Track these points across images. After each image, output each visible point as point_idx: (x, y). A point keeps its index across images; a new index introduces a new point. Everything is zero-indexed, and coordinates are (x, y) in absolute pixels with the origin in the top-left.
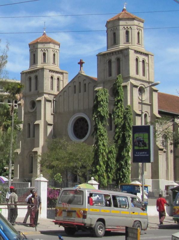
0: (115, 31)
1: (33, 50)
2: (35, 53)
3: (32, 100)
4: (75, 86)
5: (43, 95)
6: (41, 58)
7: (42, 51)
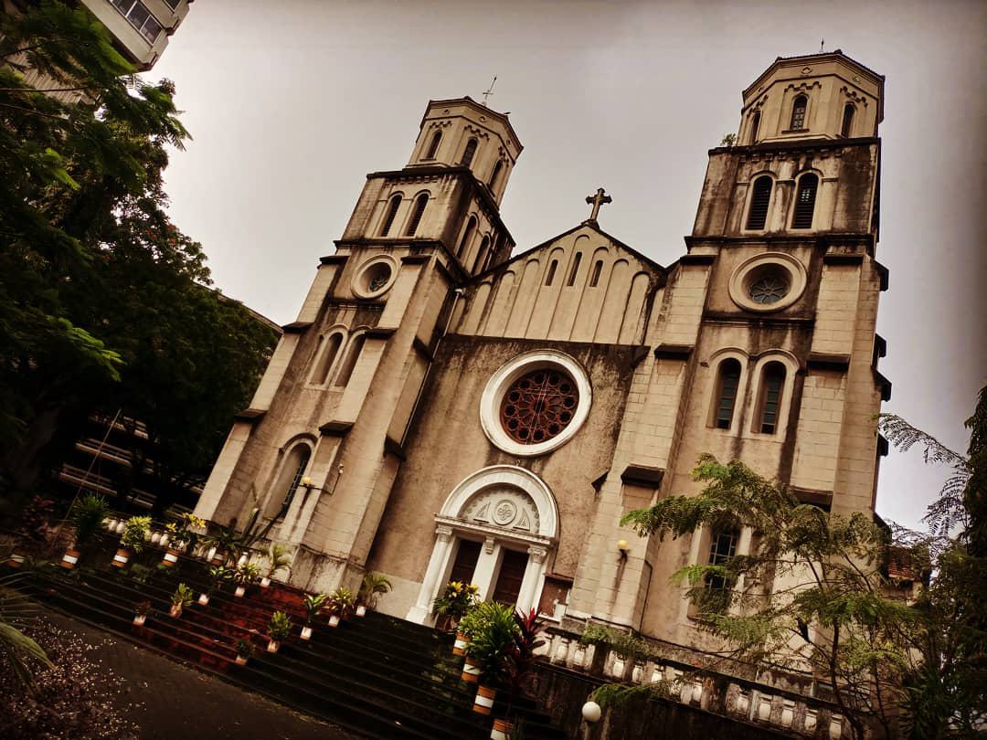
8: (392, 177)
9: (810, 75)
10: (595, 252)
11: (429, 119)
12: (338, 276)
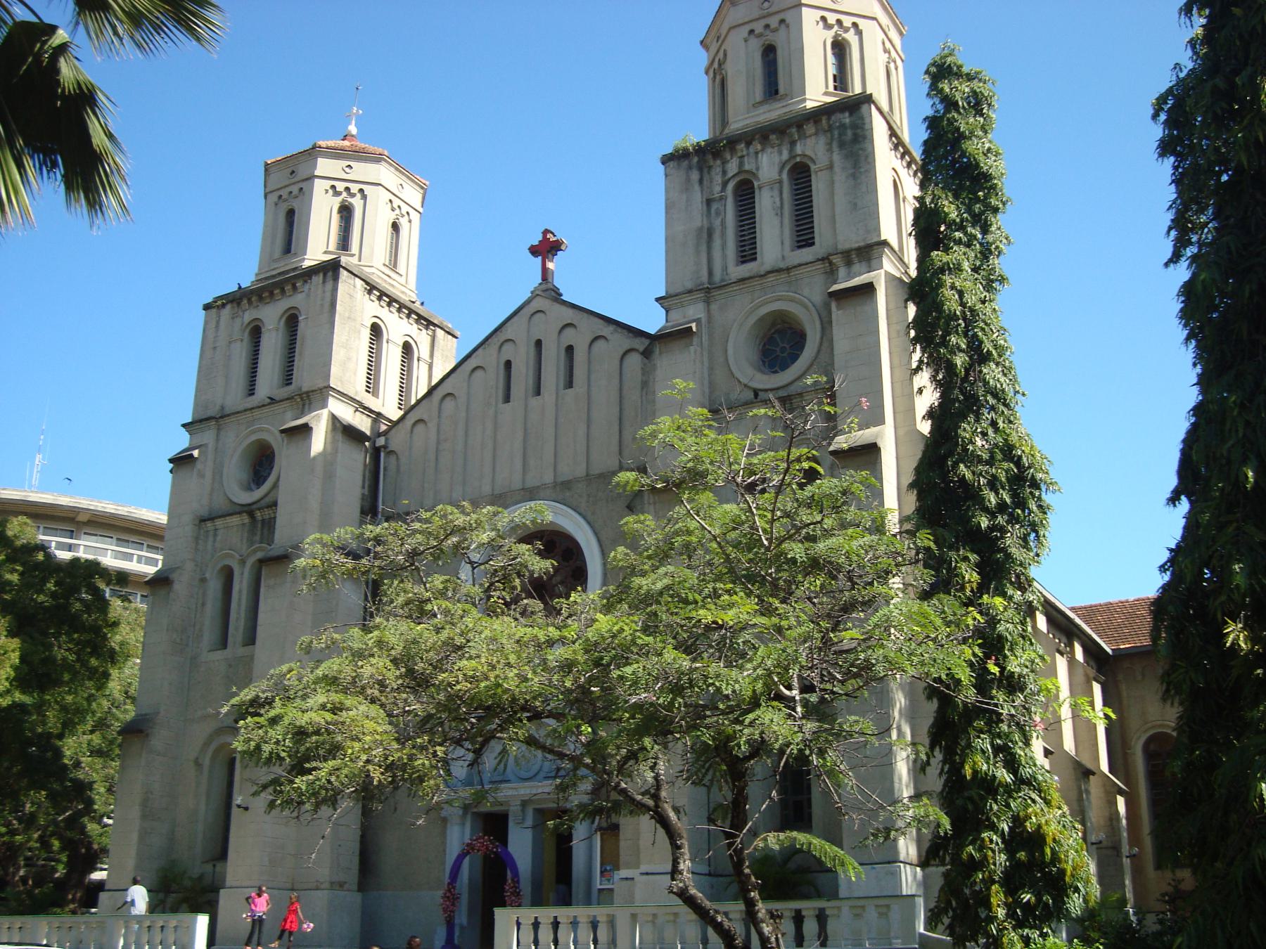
0: (770, 38)
1: (284, 193)
2: (295, 205)
3: (254, 438)
4: (508, 364)
5: (324, 405)
6: (236, 629)
7: (337, 194)
8: (237, 299)
9: (771, 10)
10: (560, 332)
11: (271, 192)
12: (269, 404)
